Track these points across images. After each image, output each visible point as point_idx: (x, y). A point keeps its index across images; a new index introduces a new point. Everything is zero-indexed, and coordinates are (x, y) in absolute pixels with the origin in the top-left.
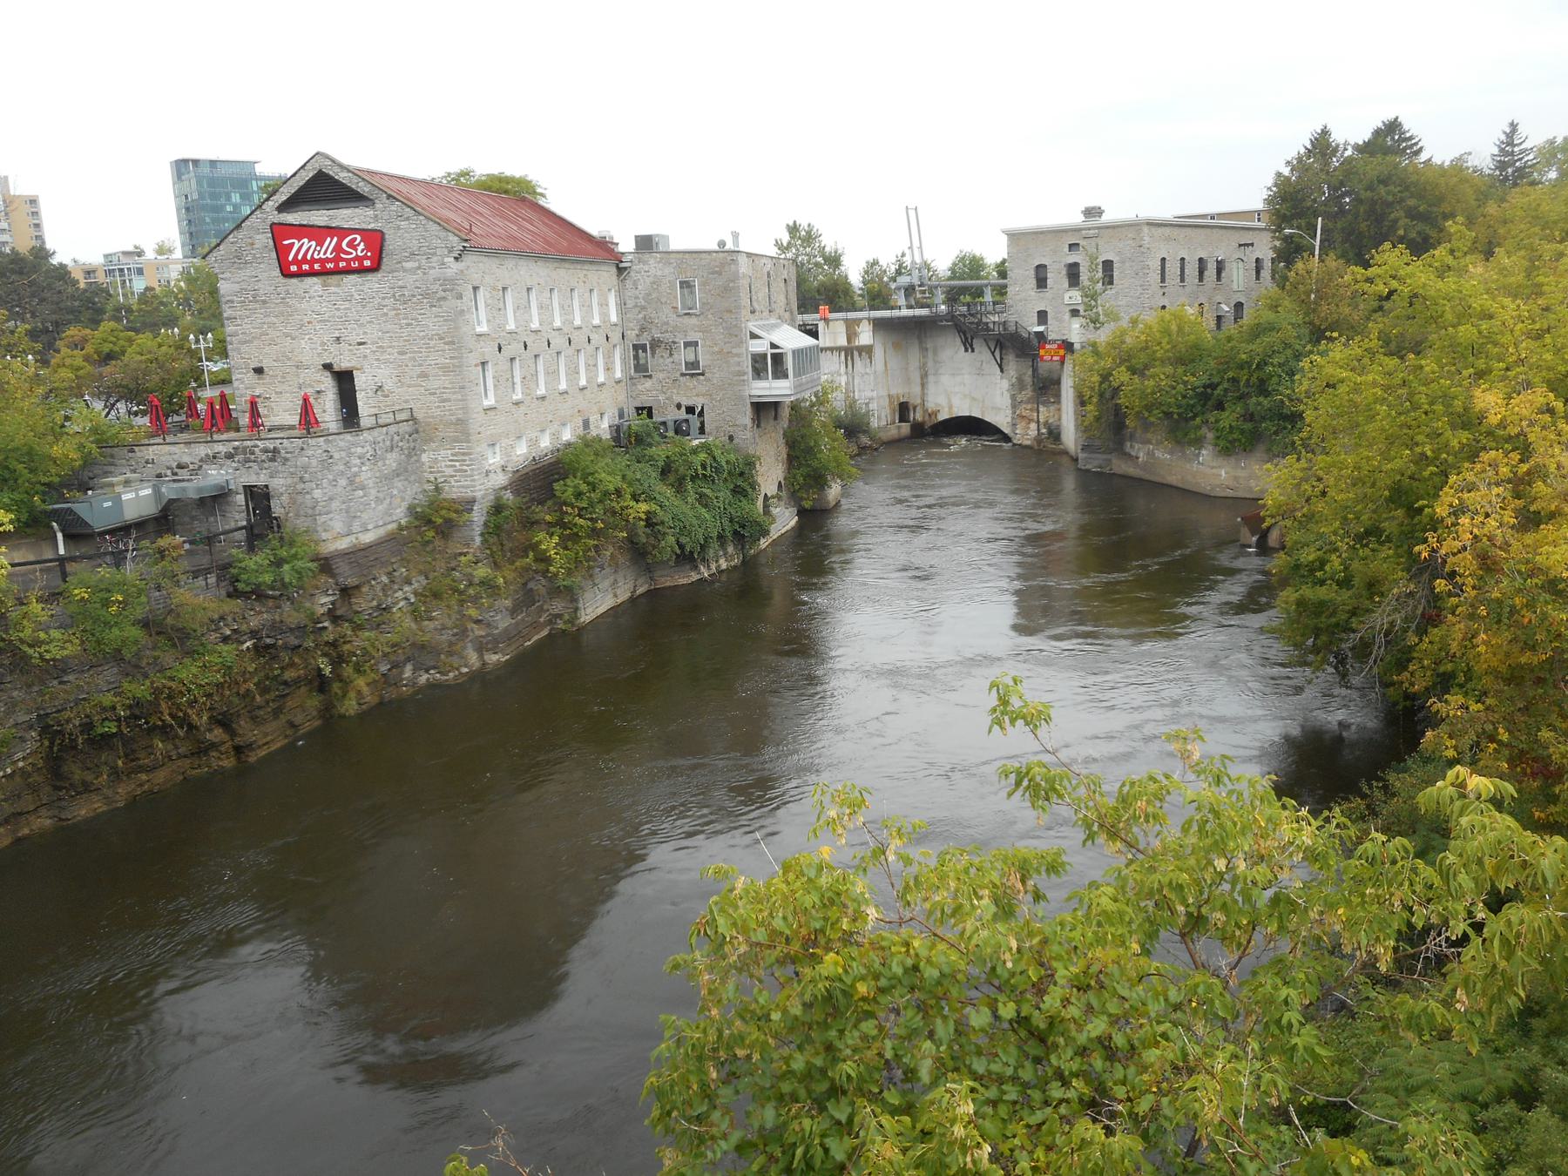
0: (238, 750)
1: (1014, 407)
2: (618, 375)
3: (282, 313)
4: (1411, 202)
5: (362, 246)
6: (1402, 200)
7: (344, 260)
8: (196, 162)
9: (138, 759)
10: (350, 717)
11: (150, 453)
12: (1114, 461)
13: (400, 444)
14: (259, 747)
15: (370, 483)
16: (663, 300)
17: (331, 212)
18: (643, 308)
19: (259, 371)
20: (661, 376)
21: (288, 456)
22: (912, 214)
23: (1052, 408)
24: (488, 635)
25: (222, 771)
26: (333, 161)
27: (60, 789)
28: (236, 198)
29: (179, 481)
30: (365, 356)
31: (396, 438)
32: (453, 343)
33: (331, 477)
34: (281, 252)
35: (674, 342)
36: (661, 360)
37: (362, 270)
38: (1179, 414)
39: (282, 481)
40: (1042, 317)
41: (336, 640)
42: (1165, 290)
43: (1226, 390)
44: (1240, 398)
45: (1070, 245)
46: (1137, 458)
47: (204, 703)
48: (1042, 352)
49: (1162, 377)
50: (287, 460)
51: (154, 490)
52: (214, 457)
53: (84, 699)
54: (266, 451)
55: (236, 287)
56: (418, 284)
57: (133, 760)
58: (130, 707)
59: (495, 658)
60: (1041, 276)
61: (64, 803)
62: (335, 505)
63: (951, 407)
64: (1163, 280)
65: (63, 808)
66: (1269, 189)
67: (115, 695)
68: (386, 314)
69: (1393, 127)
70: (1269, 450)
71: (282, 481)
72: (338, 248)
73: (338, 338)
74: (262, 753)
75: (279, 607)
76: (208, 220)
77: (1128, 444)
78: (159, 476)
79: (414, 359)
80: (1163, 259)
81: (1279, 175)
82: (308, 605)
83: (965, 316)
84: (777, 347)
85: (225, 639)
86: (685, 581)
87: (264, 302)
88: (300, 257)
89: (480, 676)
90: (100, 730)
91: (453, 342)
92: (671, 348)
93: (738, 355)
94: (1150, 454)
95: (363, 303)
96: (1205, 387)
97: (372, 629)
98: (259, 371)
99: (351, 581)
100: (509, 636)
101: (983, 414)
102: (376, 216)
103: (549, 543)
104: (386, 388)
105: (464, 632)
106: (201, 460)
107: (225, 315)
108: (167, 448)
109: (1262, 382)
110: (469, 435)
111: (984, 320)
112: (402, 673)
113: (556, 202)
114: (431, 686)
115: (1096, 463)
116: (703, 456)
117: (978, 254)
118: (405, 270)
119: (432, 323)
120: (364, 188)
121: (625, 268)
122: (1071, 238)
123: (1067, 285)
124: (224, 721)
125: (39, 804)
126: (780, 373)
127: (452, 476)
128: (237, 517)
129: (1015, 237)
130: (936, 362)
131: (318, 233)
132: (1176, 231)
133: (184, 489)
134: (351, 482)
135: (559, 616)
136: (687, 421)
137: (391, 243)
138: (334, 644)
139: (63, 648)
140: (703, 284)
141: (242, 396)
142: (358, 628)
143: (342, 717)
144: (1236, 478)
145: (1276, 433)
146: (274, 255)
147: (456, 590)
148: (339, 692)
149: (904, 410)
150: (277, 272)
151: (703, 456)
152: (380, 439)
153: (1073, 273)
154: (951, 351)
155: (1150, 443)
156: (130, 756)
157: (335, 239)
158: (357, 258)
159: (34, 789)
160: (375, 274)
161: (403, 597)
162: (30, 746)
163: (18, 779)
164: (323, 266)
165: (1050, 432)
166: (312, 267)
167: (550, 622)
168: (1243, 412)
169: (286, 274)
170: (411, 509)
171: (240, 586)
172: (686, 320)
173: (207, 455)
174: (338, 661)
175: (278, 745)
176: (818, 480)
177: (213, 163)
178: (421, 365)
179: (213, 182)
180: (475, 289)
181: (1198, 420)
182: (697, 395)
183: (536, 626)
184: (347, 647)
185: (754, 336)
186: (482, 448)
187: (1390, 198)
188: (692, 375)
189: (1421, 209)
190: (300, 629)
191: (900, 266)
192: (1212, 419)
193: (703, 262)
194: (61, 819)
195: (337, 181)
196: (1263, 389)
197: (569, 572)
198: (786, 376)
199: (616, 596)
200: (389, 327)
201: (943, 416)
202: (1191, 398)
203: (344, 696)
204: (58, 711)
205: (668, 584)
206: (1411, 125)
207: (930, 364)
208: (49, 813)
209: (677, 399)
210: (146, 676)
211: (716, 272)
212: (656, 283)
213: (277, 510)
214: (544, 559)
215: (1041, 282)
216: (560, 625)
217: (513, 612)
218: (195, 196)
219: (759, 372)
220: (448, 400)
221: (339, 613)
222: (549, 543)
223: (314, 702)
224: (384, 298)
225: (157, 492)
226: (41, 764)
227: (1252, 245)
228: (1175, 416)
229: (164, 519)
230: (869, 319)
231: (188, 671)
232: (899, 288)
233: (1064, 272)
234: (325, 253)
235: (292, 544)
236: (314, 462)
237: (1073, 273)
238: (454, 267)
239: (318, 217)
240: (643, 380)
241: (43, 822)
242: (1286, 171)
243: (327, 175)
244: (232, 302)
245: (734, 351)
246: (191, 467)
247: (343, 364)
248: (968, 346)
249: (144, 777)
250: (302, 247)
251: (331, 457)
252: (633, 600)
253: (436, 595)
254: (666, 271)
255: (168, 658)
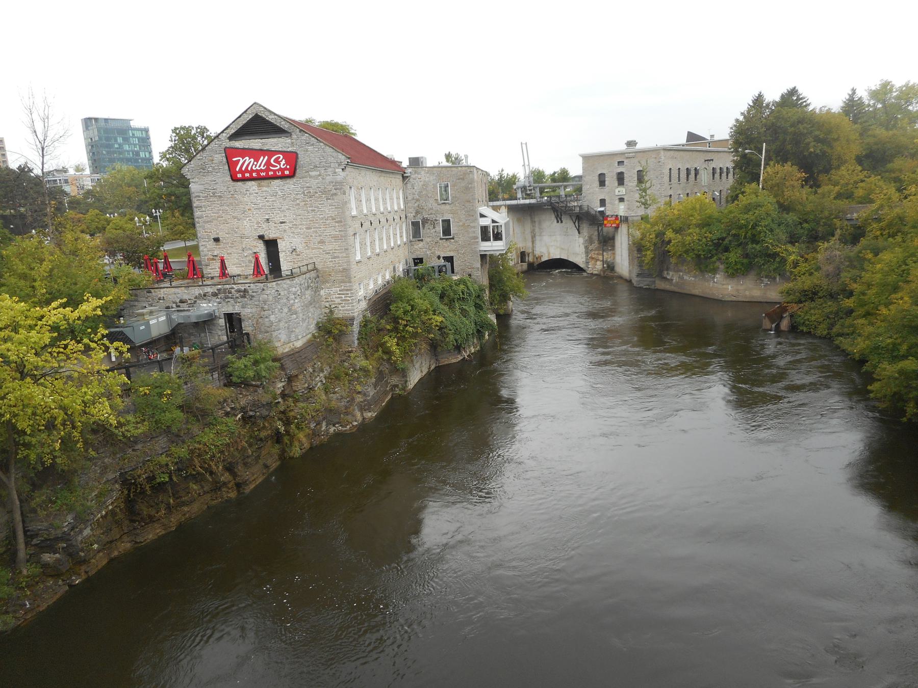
0: (238, 486)
1: (587, 253)
2: (405, 240)
3: (231, 204)
4: (817, 133)
5: (284, 162)
6: (811, 132)
7: (272, 170)
8: (96, 119)
9: (181, 497)
10: (296, 458)
11: (162, 293)
12: (656, 282)
13: (311, 285)
14: (250, 482)
15: (299, 310)
16: (429, 195)
17: (263, 140)
18: (417, 200)
19: (217, 240)
20: (429, 240)
21: (254, 294)
22: (524, 146)
23: (610, 253)
24: (365, 401)
25: (229, 501)
26: (265, 108)
27: (134, 521)
28: (120, 140)
29: (181, 311)
30: (285, 231)
31: (310, 281)
32: (341, 222)
33: (279, 307)
34: (231, 165)
35: (436, 220)
36: (428, 231)
37: (283, 177)
38: (704, 255)
39: (249, 310)
40: (603, 202)
41: (285, 410)
42: (671, 186)
43: (730, 241)
44: (739, 245)
45: (618, 162)
46: (672, 280)
47: (220, 458)
48: (605, 222)
49: (694, 234)
50: (253, 296)
51: (167, 317)
52: (205, 295)
53: (148, 461)
54: (239, 291)
55: (202, 187)
56: (319, 185)
57: (177, 498)
58: (176, 463)
59: (369, 414)
60: (601, 180)
61: (138, 531)
62: (282, 324)
63: (549, 254)
64: (670, 181)
65: (137, 535)
66: (731, 128)
67: (167, 456)
68: (299, 204)
69: (793, 92)
70: (759, 274)
71: (249, 310)
72: (268, 163)
73: (268, 219)
74: (252, 486)
75: (256, 391)
76: (104, 152)
77: (666, 272)
78: (168, 308)
79: (316, 232)
80: (670, 169)
81: (737, 120)
82: (271, 389)
83: (558, 203)
84: (497, 222)
85: (227, 414)
86: (454, 361)
87: (220, 197)
88: (243, 169)
89: (364, 427)
90: (158, 480)
91: (341, 220)
92: (434, 223)
93: (474, 227)
94: (681, 278)
95: (284, 197)
96: (719, 239)
97: (304, 401)
98: (217, 240)
99: (294, 372)
100: (376, 400)
101: (560, 256)
102: (292, 143)
103: (392, 343)
104: (298, 250)
105: (353, 399)
106: (196, 297)
107: (195, 205)
108: (173, 290)
109: (754, 235)
110: (350, 278)
111: (568, 205)
112: (321, 427)
113: (362, 137)
114: (337, 435)
115: (646, 283)
116: (462, 287)
117: (541, 169)
118: (311, 177)
119: (328, 210)
120: (285, 126)
121: (407, 177)
122: (620, 158)
123: (616, 184)
124: (230, 469)
125: (122, 533)
126: (498, 237)
127: (340, 304)
128: (220, 333)
129: (587, 159)
130: (540, 228)
131: (255, 154)
132: (677, 153)
133: (189, 317)
134: (290, 310)
135: (397, 386)
136: (445, 266)
137: (302, 159)
138: (283, 412)
139: (137, 428)
140: (453, 186)
141: (205, 256)
142: (296, 401)
143: (292, 458)
144: (738, 290)
145: (763, 264)
146: (226, 167)
147: (347, 374)
148: (288, 442)
149: (523, 255)
150: (229, 178)
151: (462, 287)
152: (302, 282)
153: (621, 178)
154: (549, 223)
155: (681, 271)
156: (176, 495)
157: (266, 157)
158: (281, 169)
159: (118, 523)
160: (292, 179)
161: (319, 381)
162: (115, 495)
163: (109, 517)
164: (243, 175)
165: (608, 266)
166: (251, 174)
167: (392, 390)
168: (742, 253)
169: (234, 179)
170: (319, 327)
171: (234, 379)
172: (443, 207)
173: (200, 294)
174: (287, 423)
175: (260, 480)
176: (505, 298)
177: (106, 120)
178: (320, 236)
179: (107, 131)
180: (350, 187)
181: (714, 259)
182: (450, 251)
183: (386, 393)
184: (292, 414)
185: (482, 216)
186: (356, 286)
187: (805, 131)
188: (447, 239)
189: (821, 137)
190: (269, 405)
191: (501, 176)
192: (724, 258)
193: (454, 173)
194: (136, 543)
195: (268, 121)
196: (755, 240)
197: (403, 362)
198: (501, 239)
199: (422, 372)
200: (300, 212)
201: (545, 259)
202: (710, 246)
203: (291, 445)
204: (134, 470)
205: (446, 363)
206: (803, 91)
207: (537, 230)
208: (129, 539)
209: (438, 253)
210: (183, 442)
211: (461, 179)
212: (425, 185)
213: (247, 327)
214: (388, 352)
215: (602, 183)
216: (397, 391)
217: (375, 386)
218: (97, 138)
219: (485, 236)
220: (338, 257)
221: (286, 392)
222: (392, 343)
223: (276, 450)
224: (297, 194)
225: (169, 319)
226: (122, 505)
227: (712, 160)
228: (702, 256)
229: (173, 337)
230: (505, 206)
231: (208, 437)
232: (518, 188)
233: (615, 177)
234: (260, 166)
235: (261, 350)
236: (271, 298)
237: (621, 178)
238: (341, 175)
239: (255, 143)
240: (418, 242)
241: (125, 546)
242: (741, 118)
243: (261, 117)
244: (199, 197)
245: (471, 224)
246: (189, 302)
247: (270, 235)
248: (559, 219)
249: (186, 509)
250: (245, 162)
251: (280, 294)
252: (429, 373)
253: (338, 378)
254: (431, 178)
255: (195, 429)
